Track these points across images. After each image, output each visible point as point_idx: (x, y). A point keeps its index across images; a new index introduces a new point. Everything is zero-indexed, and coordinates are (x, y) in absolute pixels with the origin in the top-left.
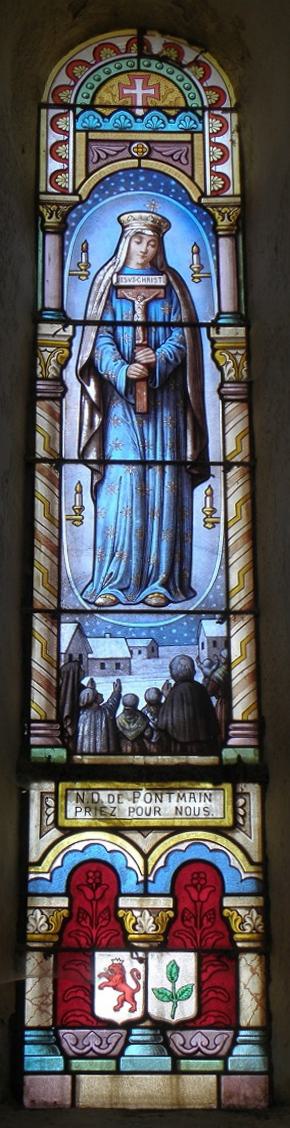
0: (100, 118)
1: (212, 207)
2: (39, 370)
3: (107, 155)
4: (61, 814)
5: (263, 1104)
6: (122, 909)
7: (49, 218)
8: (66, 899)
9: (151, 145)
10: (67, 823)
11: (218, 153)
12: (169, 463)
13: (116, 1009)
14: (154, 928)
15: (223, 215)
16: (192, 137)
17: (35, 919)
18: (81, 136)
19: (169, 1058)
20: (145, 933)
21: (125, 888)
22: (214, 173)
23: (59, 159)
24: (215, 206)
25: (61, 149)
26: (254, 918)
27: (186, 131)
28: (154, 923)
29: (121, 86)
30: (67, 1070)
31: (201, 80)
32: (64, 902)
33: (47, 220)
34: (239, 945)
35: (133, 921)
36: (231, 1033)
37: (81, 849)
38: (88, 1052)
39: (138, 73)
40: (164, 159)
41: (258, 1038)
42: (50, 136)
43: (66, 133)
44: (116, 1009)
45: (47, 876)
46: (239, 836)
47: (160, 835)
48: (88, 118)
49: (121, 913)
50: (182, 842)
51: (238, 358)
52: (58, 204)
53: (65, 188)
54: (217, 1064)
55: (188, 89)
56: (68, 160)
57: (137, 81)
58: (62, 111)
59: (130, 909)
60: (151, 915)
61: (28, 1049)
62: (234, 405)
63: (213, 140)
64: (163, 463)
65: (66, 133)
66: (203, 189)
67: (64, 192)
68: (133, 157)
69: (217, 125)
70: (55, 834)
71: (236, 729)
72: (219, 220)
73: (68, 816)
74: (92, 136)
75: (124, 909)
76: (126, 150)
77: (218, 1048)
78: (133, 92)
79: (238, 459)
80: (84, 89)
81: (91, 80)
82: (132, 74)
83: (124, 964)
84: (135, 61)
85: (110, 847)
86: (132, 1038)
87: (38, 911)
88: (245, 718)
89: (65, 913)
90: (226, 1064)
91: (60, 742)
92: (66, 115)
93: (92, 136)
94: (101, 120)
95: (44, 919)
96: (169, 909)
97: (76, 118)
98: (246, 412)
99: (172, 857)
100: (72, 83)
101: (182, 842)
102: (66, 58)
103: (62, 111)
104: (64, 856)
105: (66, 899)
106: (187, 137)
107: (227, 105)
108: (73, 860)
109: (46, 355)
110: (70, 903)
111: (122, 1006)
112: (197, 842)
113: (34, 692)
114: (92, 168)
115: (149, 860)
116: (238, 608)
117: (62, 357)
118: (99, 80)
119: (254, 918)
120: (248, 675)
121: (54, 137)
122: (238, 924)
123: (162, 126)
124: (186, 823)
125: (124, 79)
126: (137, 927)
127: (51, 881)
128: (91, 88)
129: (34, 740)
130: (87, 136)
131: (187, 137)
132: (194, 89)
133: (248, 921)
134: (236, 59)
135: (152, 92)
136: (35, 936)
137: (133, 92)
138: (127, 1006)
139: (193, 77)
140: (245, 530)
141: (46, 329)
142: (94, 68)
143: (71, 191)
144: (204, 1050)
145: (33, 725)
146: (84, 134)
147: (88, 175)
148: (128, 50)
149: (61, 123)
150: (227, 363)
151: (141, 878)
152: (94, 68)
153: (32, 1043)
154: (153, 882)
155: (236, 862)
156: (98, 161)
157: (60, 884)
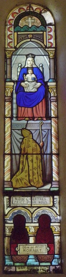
1: (48, 51)
2: (6, 94)
3: (22, 38)
4: (11, 203)
6: (26, 226)
7: (8, 55)
8: (38, 224)
9: (33, 35)
10: (14, 205)
11: (50, 37)
14: (34, 231)
15: (50, 52)
16: (43, 33)
18: (16, 34)
19: (38, 262)
20: (32, 232)
21: (52, 221)
23: (10, 39)
25: (10, 36)
26: (58, 228)
27: (42, 31)
28: (34, 230)
32: (37, 225)
33: (50, 55)
34: (29, 235)
35: (55, 229)
36: (53, 256)
40: (36, 39)
42: (52, 34)
43: (12, 32)
46: (55, 209)
47: (37, 208)
49: (26, 227)
51: (55, 90)
52: (10, 51)
53: (12, 47)
56: (12, 39)
58: (11, 26)
59: (28, 226)
60: (33, 228)
61: (6, 260)
62: (8, 103)
63: (48, 33)
67: (12, 48)
68: (29, 38)
71: (54, 183)
72: (7, 54)
73: (13, 203)
74: (19, 33)
77: (50, 259)
85: (41, 211)
86: (29, 258)
88: (7, 180)
89: (38, 227)
92: (12, 27)
93: (19, 33)
96: (38, 226)
98: (11, 105)
100: (13, 18)
102: (11, 12)
103: (11, 26)
105: (38, 224)
106: (42, 33)
109: (7, 90)
113: (53, 174)
114: (19, 41)
116: (7, 153)
117: (11, 91)
119: (58, 228)
121: (9, 33)
122: (54, 230)
123: (36, 30)
124: (43, 205)
126: (30, 231)
129: (5, 186)
130: (17, 33)
131: (42, 33)
133: (57, 229)
135: (33, 21)
140: (10, 134)
141: (7, 84)
143: (13, 47)
145: (5, 182)
147: (18, 44)
149: (10, 29)
153: (7, 259)
156: (20, 40)
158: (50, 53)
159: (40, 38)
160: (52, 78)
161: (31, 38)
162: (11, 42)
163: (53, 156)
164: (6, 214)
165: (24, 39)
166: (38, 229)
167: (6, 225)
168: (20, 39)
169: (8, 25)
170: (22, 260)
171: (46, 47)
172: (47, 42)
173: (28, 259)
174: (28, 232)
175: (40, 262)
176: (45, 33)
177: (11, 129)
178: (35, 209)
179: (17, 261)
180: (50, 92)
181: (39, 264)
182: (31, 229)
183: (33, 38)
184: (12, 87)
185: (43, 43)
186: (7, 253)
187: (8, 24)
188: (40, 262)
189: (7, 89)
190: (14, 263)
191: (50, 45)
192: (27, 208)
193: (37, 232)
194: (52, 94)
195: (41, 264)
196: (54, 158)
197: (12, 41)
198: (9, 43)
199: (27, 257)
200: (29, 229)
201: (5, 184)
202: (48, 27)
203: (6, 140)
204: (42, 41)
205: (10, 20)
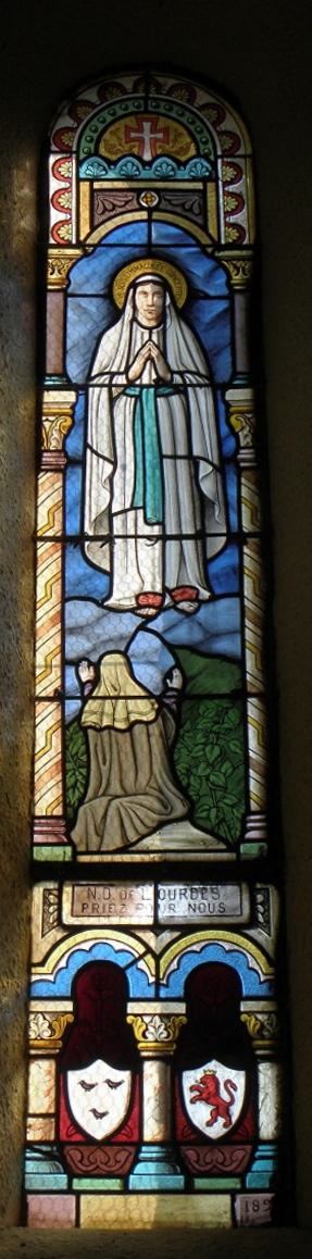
0: (174, 164)
3: (114, 206)
5: (270, 1219)
7: (52, 274)
11: (233, 204)
12: (188, 537)
13: (209, 1124)
15: (235, 267)
16: (205, 186)
17: (37, 1024)
18: (85, 187)
19: (65, 1176)
22: (228, 225)
24: (229, 259)
28: (165, 1029)
29: (128, 129)
30: (70, 1191)
31: (215, 124)
32: (181, 1008)
36: (249, 1148)
37: (117, 948)
38: (212, 1169)
39: (145, 116)
41: (159, 1155)
43: (68, 179)
44: (209, 1124)
45: (51, 978)
47: (176, 934)
48: (126, 165)
49: (129, 1019)
50: (85, 941)
54: (232, 1183)
55: (201, 132)
57: (145, 124)
59: (141, 1015)
64: (180, 537)
65: (68, 179)
66: (216, 237)
68: (142, 208)
69: (230, 173)
70: (56, 934)
72: (233, 274)
74: (97, 185)
75: (135, 1015)
76: (135, 202)
77: (118, 1166)
78: (140, 135)
79: (50, 533)
80: (88, 132)
81: (95, 122)
82: (140, 116)
83: (217, 1075)
84: (142, 102)
86: (142, 1155)
87: (40, 1015)
89: (70, 1018)
90: (243, 1182)
91: (65, 840)
93: (97, 185)
94: (141, 168)
95: (47, 1024)
97: (79, 164)
99: (184, 960)
100: (76, 125)
101: (85, 941)
104: (70, 957)
106: (199, 186)
107: (241, 152)
108: (80, 960)
109: (47, 424)
110: (76, 1007)
111: (216, 1121)
112: (212, 943)
115: (161, 961)
116: (43, 694)
117: (64, 427)
118: (103, 122)
120: (56, 763)
125: (130, 121)
126: (147, 1034)
127: (54, 983)
128: (95, 131)
129: (37, 838)
130: (91, 186)
131: (199, 186)
132: (206, 134)
134: (229, 96)
135: (160, 136)
136: (36, 1042)
137: (140, 135)
138: (221, 1121)
139: (205, 120)
141: (49, 397)
142: (99, 108)
144: (221, 1167)
145: (37, 821)
146: (88, 183)
147: (93, 228)
148: (135, 90)
150: (243, 428)
151: (152, 979)
152: (99, 108)
154: (167, 986)
155: (251, 963)
156: (103, 213)
157: (64, 987)
158: (231, 269)
159: (190, 210)
160: (43, 1111)
161: (150, 210)
162: (61, 222)
163: (249, 704)
164: (81, 97)
165: (119, 210)
166: (183, 1029)
167: (36, 1006)
168: (105, 209)
169: (55, 152)
170: (222, 1164)
171: (217, 246)
172: (222, 222)
173: (137, 1161)
174: (139, 1042)
175: (72, 1175)
176: (211, 186)
177: (63, 632)
178: (167, 936)
179: (84, 1169)
180: (237, 430)
181: (70, 1183)
182: (149, 1028)
183: (108, 569)
184: (69, 411)
185: (204, 228)
186: (152, 514)
187: (54, 148)
188: (71, 1176)
189: (47, 420)
190: (71, 1176)
191: (234, 234)
192: (140, 934)
193: (178, 1041)
194: (246, 436)
195: (78, 1184)
196: (253, 710)
197: (69, 217)
198: (56, 192)
199: (249, 1151)
200: (144, 1027)
201: (36, 829)
202: (223, 162)
203: (40, 563)
204: (200, 221)
205: (57, 195)
